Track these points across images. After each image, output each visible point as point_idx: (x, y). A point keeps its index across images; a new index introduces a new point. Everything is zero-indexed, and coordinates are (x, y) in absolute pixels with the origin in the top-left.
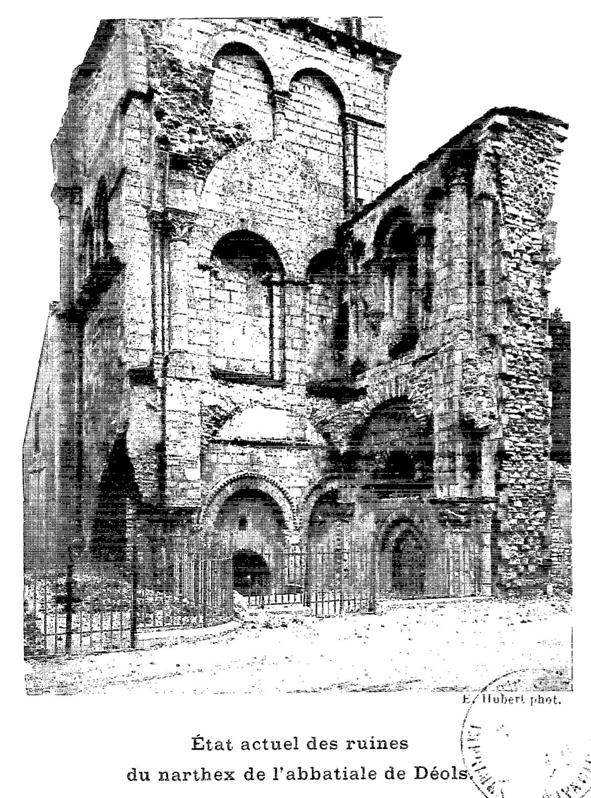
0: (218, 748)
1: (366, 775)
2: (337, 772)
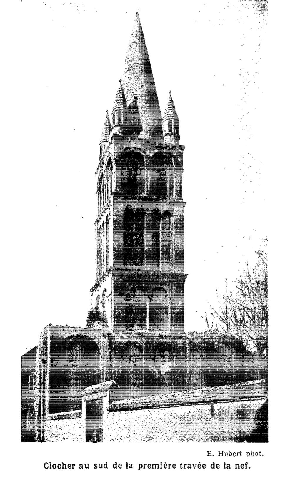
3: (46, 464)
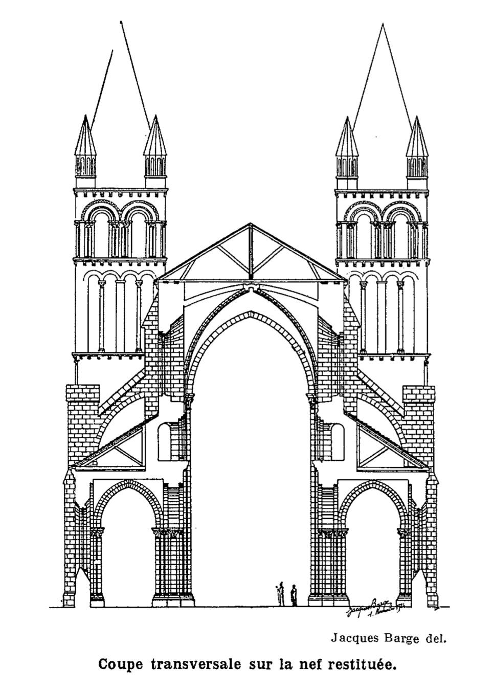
0: (167, 666)
1: (233, 666)
2: (352, 662)
3: (103, 662)
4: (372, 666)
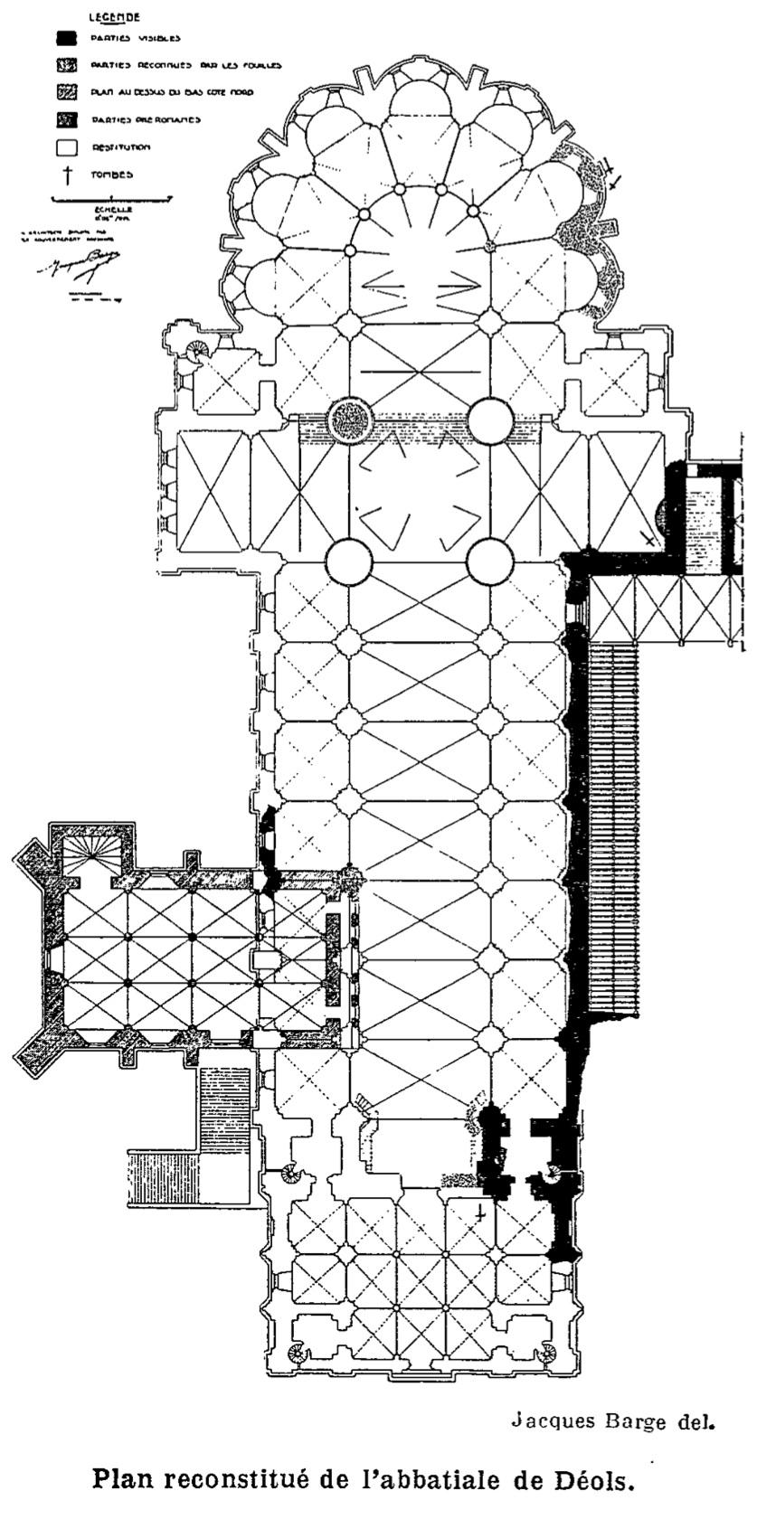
2: (253, 1475)
4: (288, 1481)
